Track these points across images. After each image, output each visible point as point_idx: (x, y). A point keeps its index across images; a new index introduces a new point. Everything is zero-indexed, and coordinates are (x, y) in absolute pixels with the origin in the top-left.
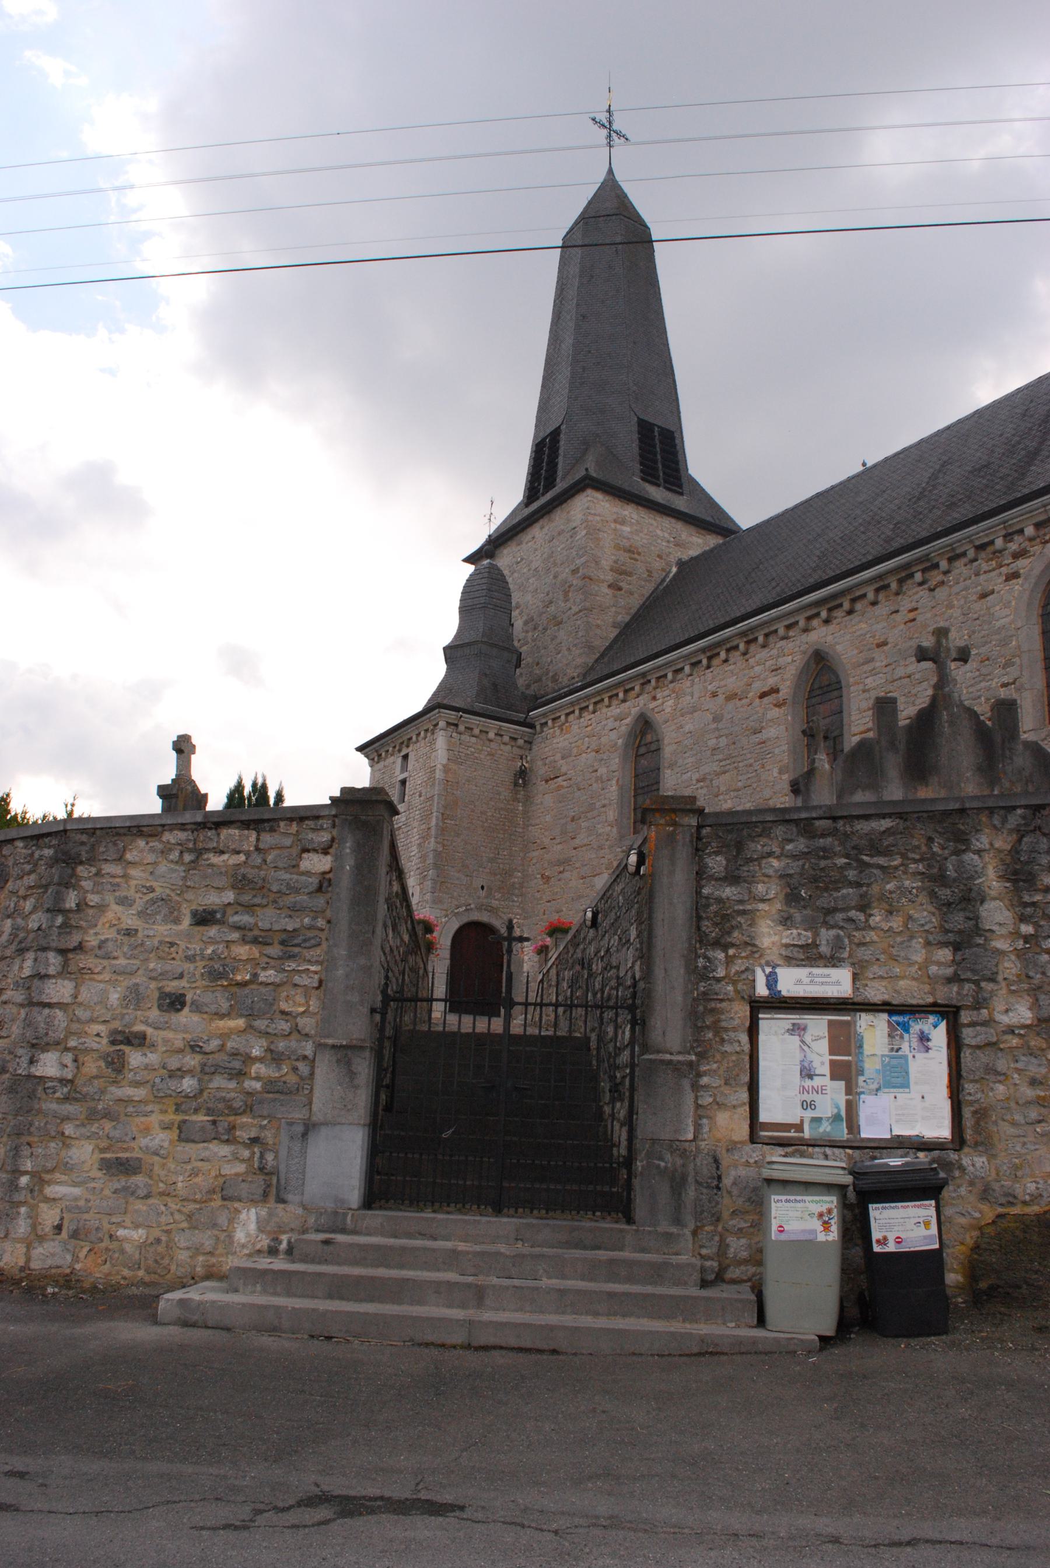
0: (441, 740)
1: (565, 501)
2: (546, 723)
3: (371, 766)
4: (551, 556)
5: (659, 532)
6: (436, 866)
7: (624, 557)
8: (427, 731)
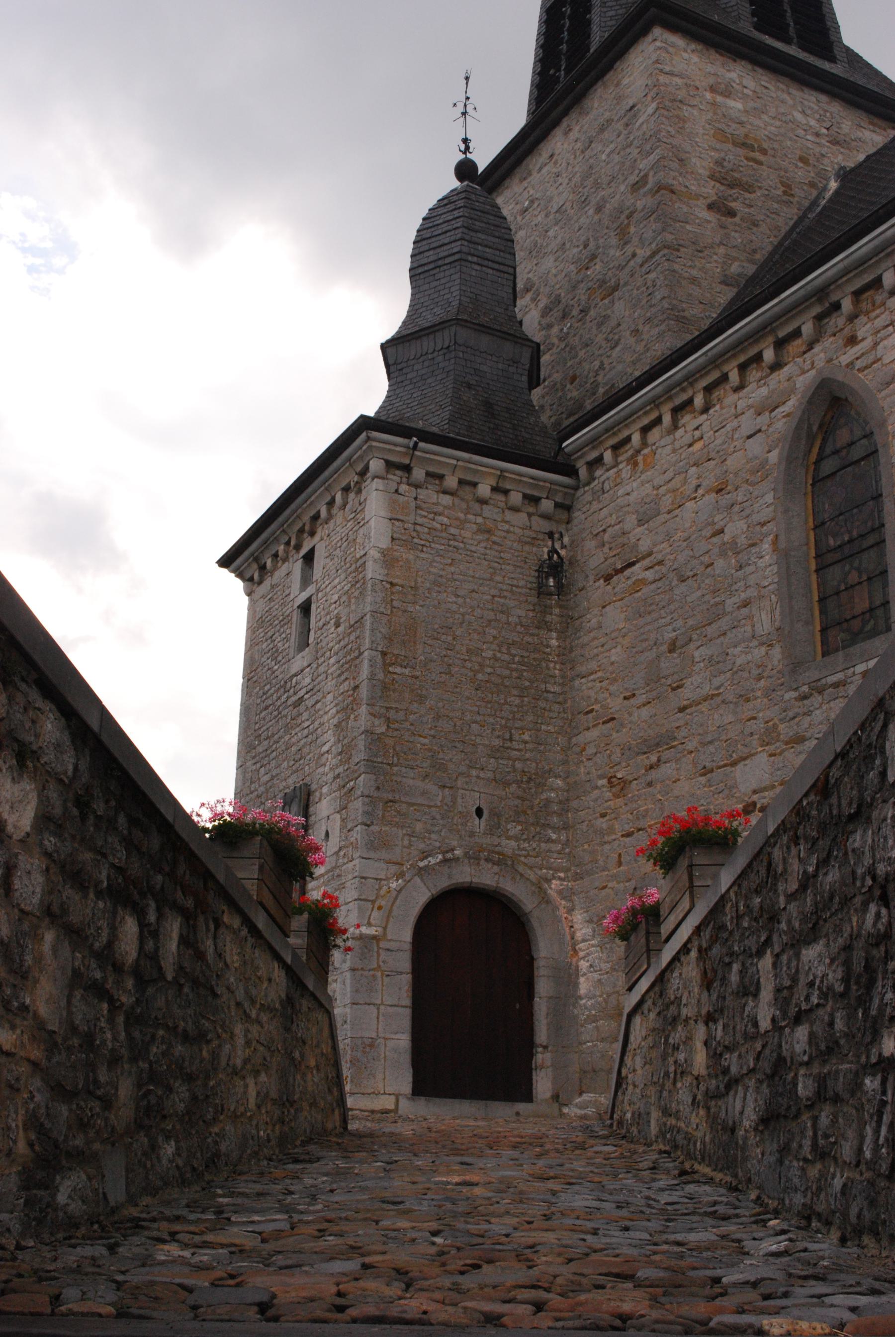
0: (375, 500)
1: (610, 67)
2: (599, 460)
3: (249, 594)
4: (586, 176)
5: (799, 117)
6: (371, 765)
7: (734, 156)
8: (346, 489)
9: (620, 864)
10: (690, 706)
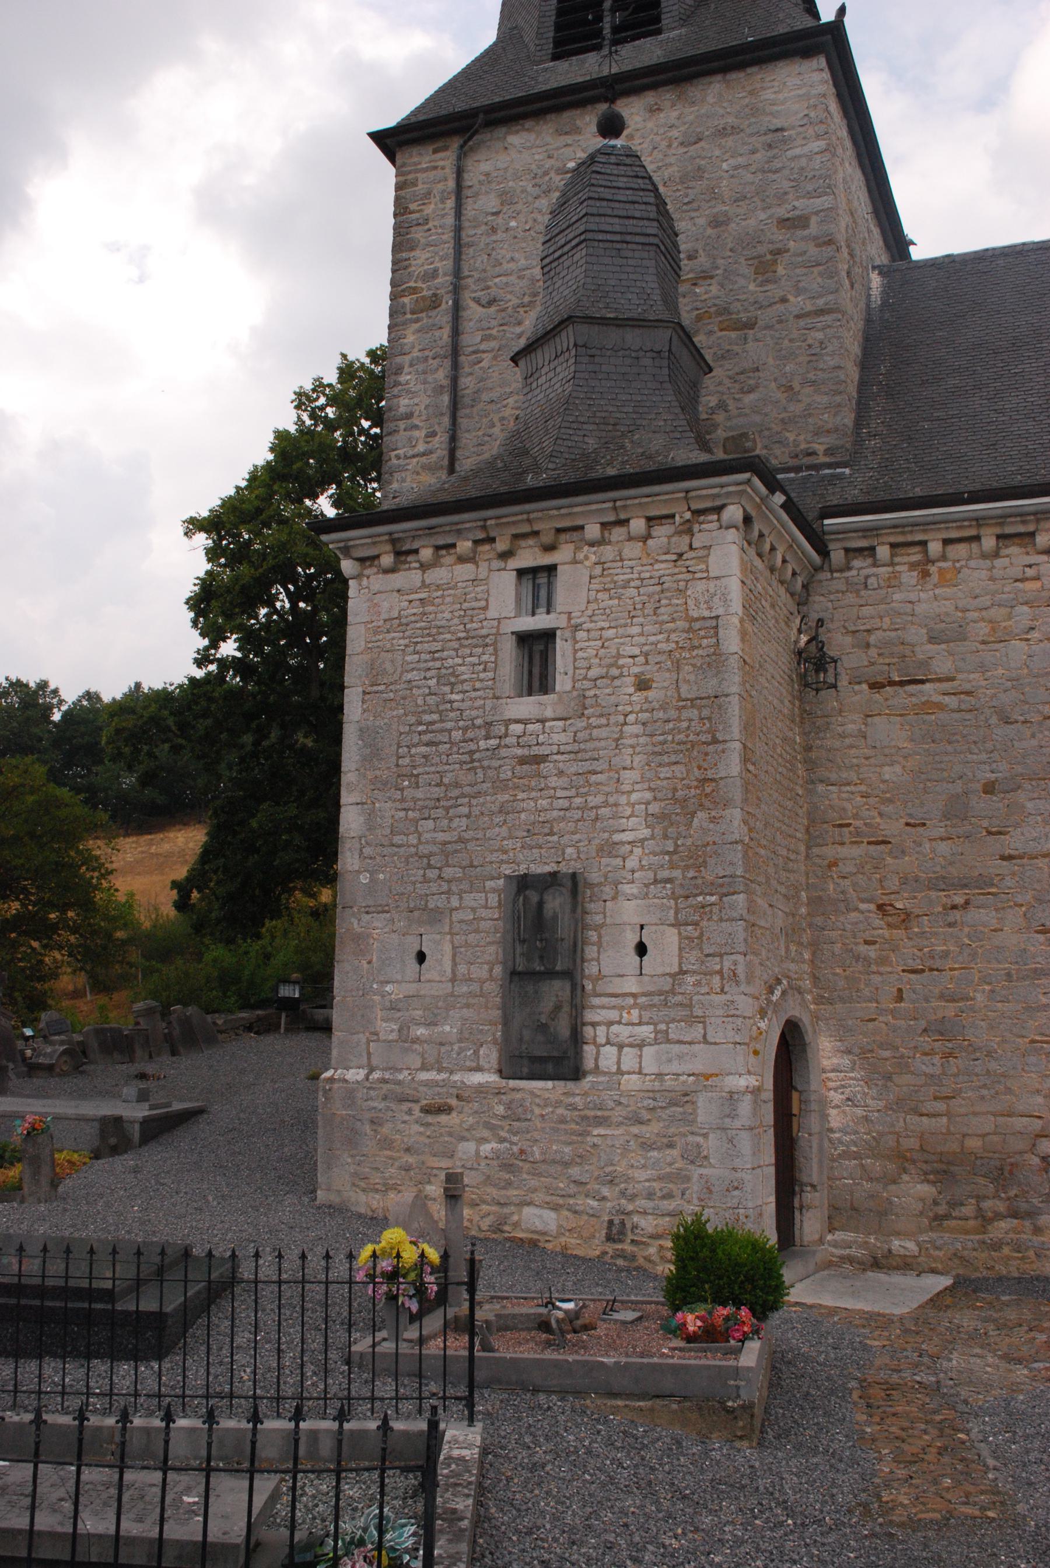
9: (900, 998)
10: (1021, 857)
